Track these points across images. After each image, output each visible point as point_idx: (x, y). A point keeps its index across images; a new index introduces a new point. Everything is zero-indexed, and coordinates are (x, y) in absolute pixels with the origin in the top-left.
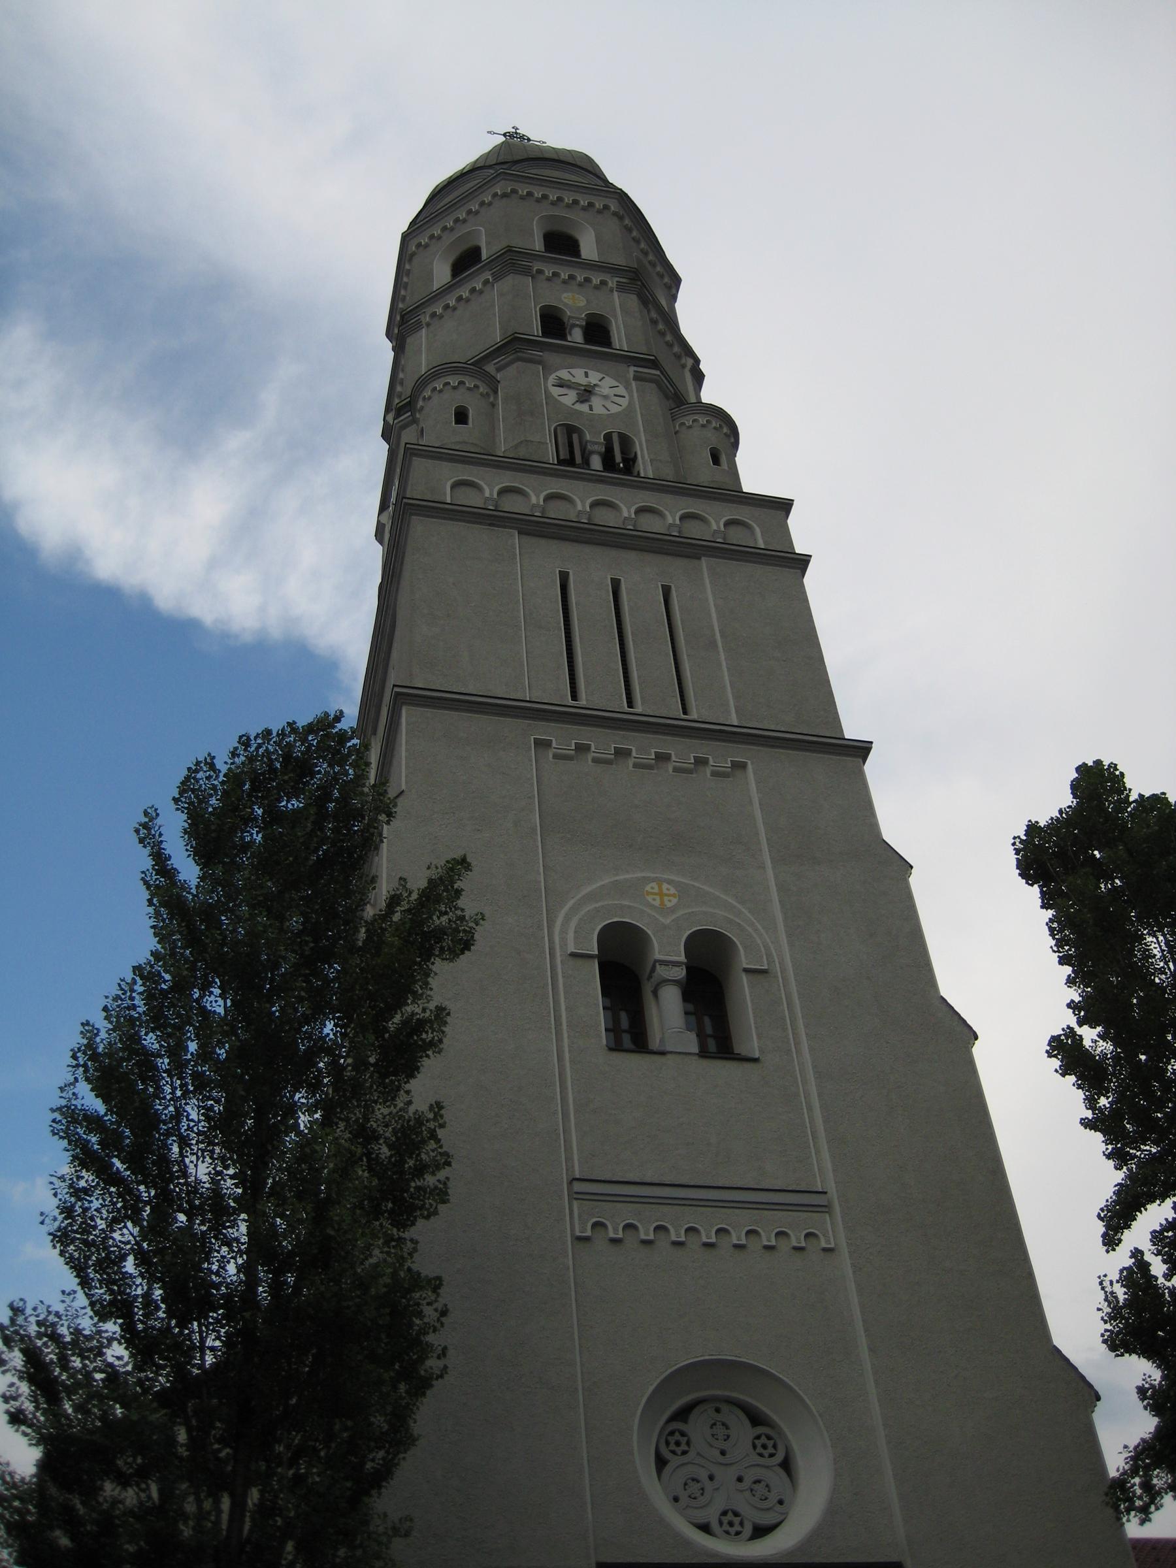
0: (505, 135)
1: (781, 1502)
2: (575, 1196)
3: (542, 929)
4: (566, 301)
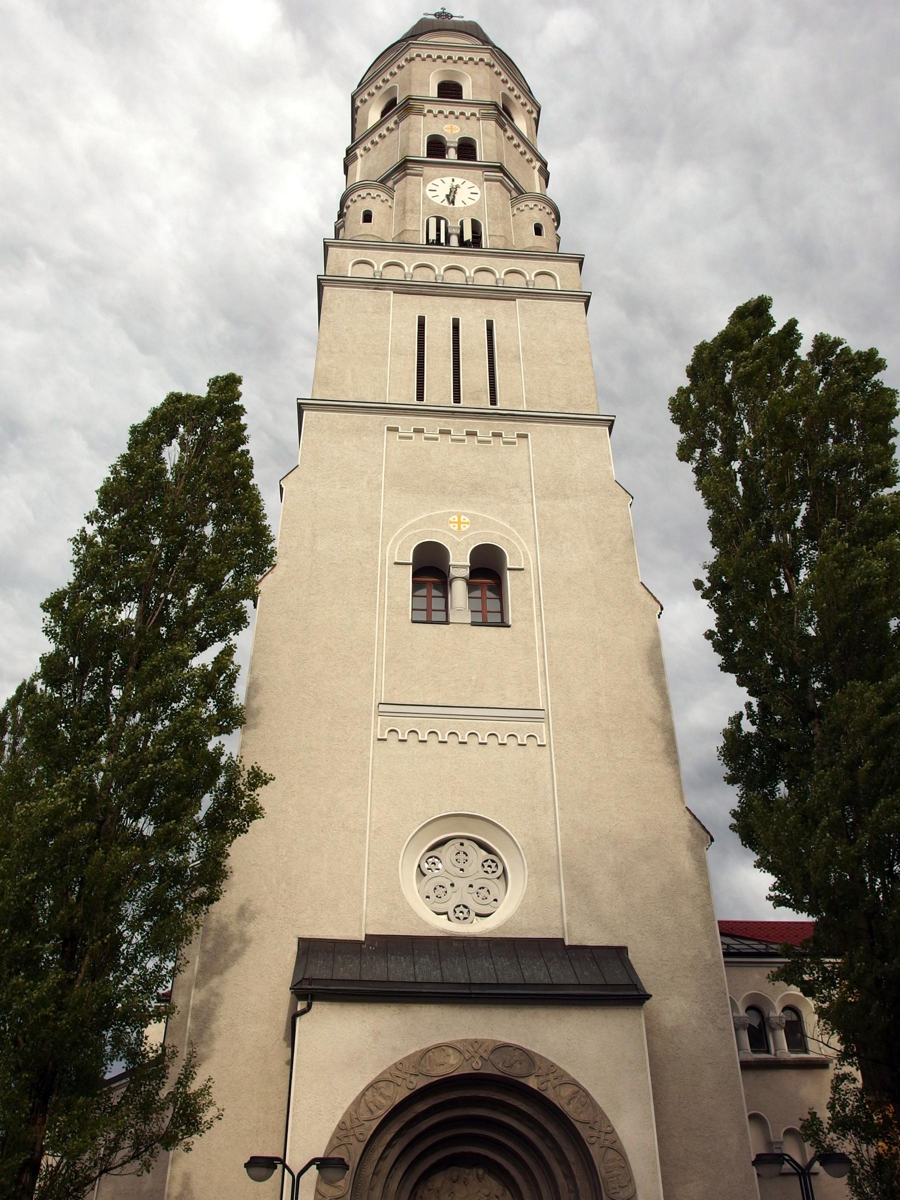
0: (435, 15)
1: (495, 900)
2: (380, 713)
3: (378, 548)
4: (446, 130)
